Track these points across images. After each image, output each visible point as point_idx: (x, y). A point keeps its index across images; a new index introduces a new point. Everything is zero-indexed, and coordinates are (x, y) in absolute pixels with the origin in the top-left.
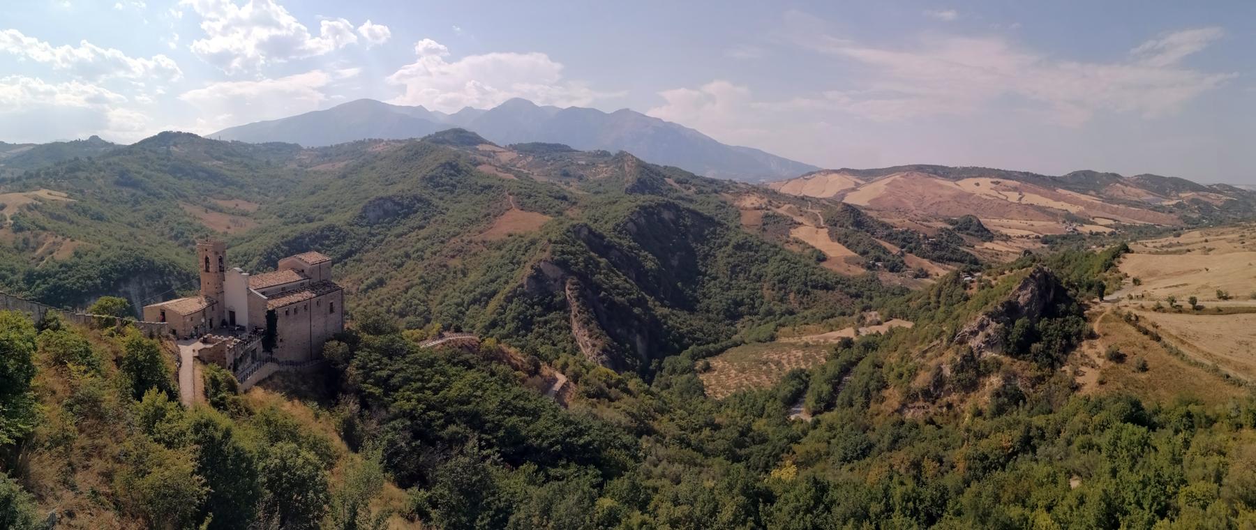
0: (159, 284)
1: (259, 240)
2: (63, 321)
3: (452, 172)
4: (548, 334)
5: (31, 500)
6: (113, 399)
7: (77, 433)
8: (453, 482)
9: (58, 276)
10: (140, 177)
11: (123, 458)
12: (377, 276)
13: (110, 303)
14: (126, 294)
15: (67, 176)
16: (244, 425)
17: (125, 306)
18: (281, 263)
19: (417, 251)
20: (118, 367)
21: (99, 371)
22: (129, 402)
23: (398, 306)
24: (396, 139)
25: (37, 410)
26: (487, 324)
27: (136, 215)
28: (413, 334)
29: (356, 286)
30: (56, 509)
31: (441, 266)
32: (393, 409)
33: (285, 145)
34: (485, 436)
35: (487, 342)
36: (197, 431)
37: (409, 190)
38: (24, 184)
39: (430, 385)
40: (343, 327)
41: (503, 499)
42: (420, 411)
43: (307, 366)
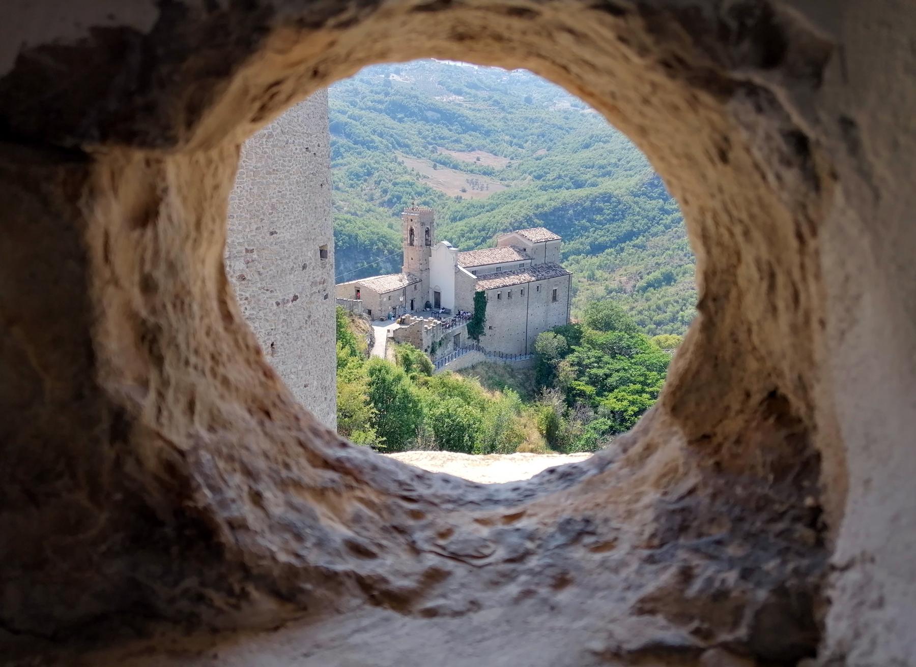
1: (503, 209)
10: (344, 119)
12: (663, 269)
28: (667, 340)
29: (632, 283)
36: (372, 374)
42: (630, 412)
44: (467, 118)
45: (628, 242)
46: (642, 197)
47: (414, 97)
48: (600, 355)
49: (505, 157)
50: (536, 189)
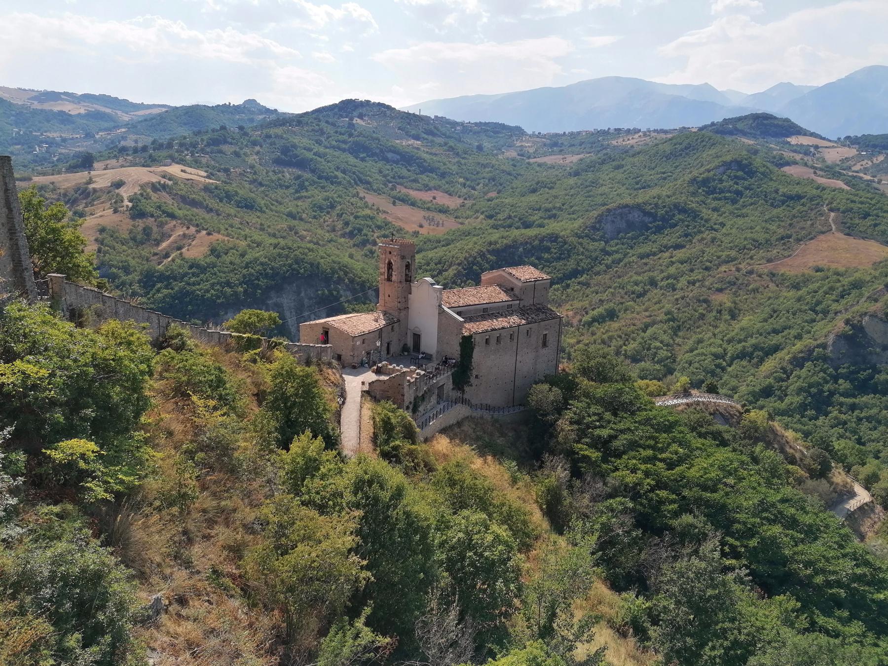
0: (323, 294)
2: (190, 338)
3: (740, 173)
4: (854, 425)
5: (130, 578)
6: (250, 447)
7: (197, 490)
8: (681, 589)
9: (186, 279)
10: (310, 155)
11: (257, 527)
12: (606, 306)
13: (254, 319)
14: (278, 307)
15: (208, 150)
16: (421, 485)
17: (275, 322)
18: (485, 276)
20: (260, 403)
21: (233, 409)
22: (271, 451)
23: (632, 346)
25: (147, 456)
26: (757, 389)
27: (300, 203)
28: (648, 386)
29: (578, 317)
30: (163, 592)
31: (699, 301)
32: (613, 480)
34: (729, 539)
35: (752, 414)
37: (669, 197)
38: (150, 156)
39: (664, 456)
40: (557, 367)
41: (745, 631)
42: (646, 487)
43: (506, 413)
44: (425, 161)
45: (573, 279)
46: (585, 239)
47: (376, 139)
48: (600, 411)
49: (459, 197)
50: (488, 228)
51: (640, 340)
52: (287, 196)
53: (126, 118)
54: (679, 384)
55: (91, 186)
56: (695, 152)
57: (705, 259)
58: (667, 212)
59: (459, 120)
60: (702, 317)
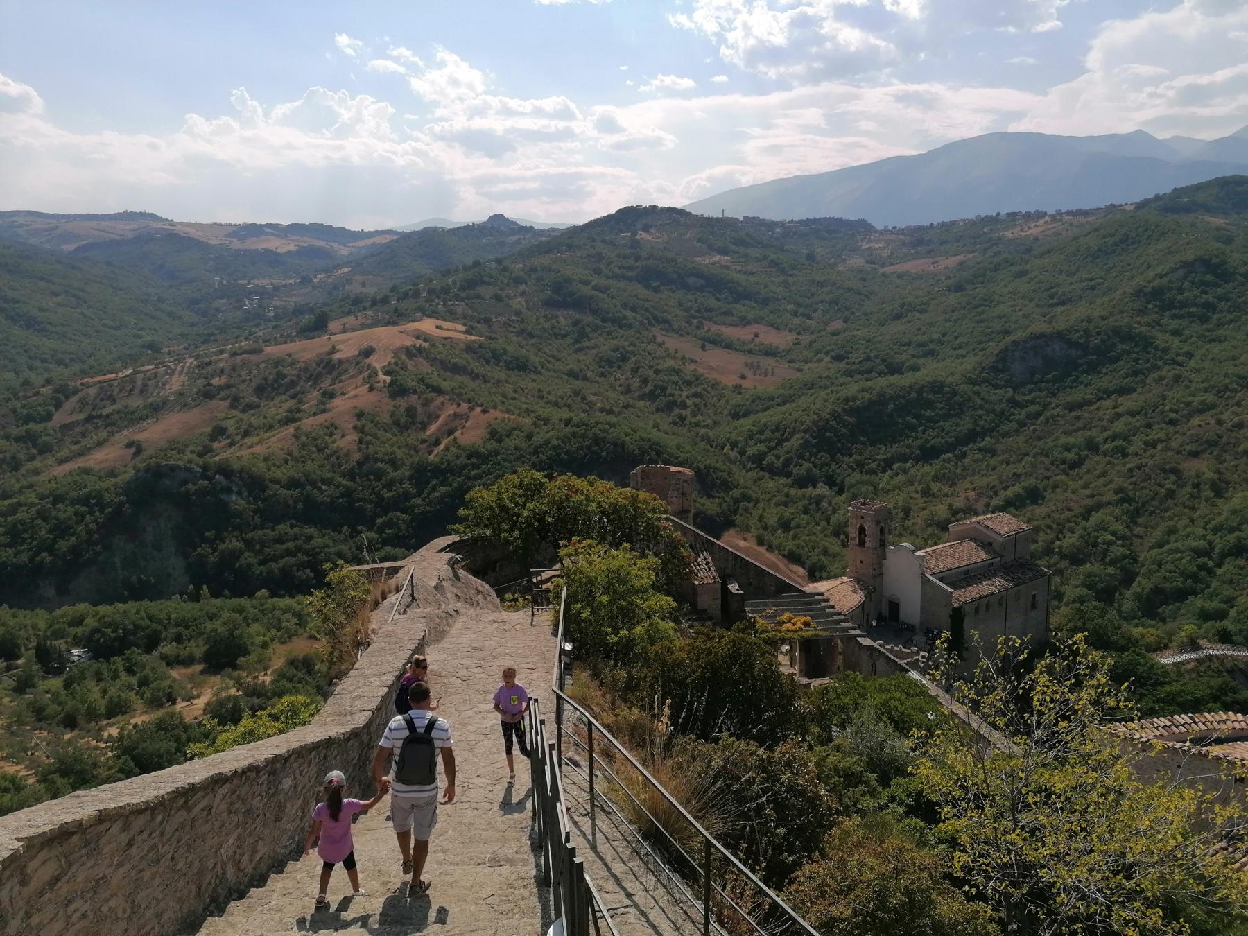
3: (1209, 277)
10: (587, 291)
15: (463, 295)
19: (1114, 438)
24: (1074, 208)
27: (581, 357)
29: (984, 500)
31: (1164, 471)
33: (840, 222)
37: (1103, 318)
45: (971, 445)
49: (790, 331)
51: (1081, 532)
52: (565, 349)
53: (344, 252)
54: (1183, 634)
55: (337, 356)
56: (1135, 246)
57: (1167, 408)
58: (1103, 341)
59: (776, 219)
60: (1171, 494)
